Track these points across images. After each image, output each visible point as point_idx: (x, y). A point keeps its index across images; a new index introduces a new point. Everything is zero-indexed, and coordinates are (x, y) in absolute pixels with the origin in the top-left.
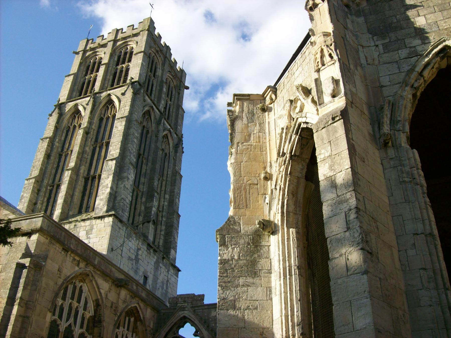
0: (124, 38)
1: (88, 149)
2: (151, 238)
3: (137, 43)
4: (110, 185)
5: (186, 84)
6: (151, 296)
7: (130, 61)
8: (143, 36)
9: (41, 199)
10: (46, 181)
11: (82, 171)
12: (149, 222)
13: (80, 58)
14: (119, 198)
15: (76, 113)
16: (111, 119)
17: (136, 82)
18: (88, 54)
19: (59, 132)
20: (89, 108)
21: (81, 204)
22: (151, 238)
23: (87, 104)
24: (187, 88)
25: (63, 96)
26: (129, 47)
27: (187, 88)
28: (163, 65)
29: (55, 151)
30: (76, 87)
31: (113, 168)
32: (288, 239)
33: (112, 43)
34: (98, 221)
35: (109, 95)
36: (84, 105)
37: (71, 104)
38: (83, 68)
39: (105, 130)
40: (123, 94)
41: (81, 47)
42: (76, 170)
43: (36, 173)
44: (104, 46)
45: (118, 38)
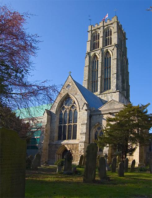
0: (107, 25)
1: (103, 69)
2: (125, 95)
3: (113, 27)
4: (116, 82)
5: (126, 38)
6: (17, 83)
7: (111, 35)
8: (115, 25)
9: (90, 86)
10: (90, 80)
12: (124, 90)
13: (90, 34)
14: (118, 86)
15: (95, 56)
17: (116, 44)
18: (93, 32)
19: (91, 64)
20: (101, 55)
21: (106, 87)
22: (125, 95)
24: (127, 39)
25: (88, 49)
27: (127, 39)
28: (121, 33)
29: (91, 70)
33: (102, 27)
35: (107, 49)
36: (98, 53)
38: (93, 38)
39: (108, 63)
40: (113, 50)
41: (90, 29)
42: (101, 77)
43: (87, 78)
44: (99, 28)
45: (104, 25)
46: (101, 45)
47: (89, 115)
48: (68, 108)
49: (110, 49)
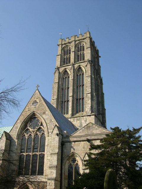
10: (60, 100)
11: (75, 96)
16: (81, 76)
18: (63, 46)
23: (71, 69)
24: (100, 57)
25: (58, 64)
26: (82, 44)
27: (100, 57)
30: (62, 60)
31: (90, 97)
32: (80, 81)
34: (89, 117)
37: (63, 68)
40: (86, 66)
42: (73, 96)
46: (72, 60)
47: (61, 141)
48: (34, 132)
49: (83, 65)
